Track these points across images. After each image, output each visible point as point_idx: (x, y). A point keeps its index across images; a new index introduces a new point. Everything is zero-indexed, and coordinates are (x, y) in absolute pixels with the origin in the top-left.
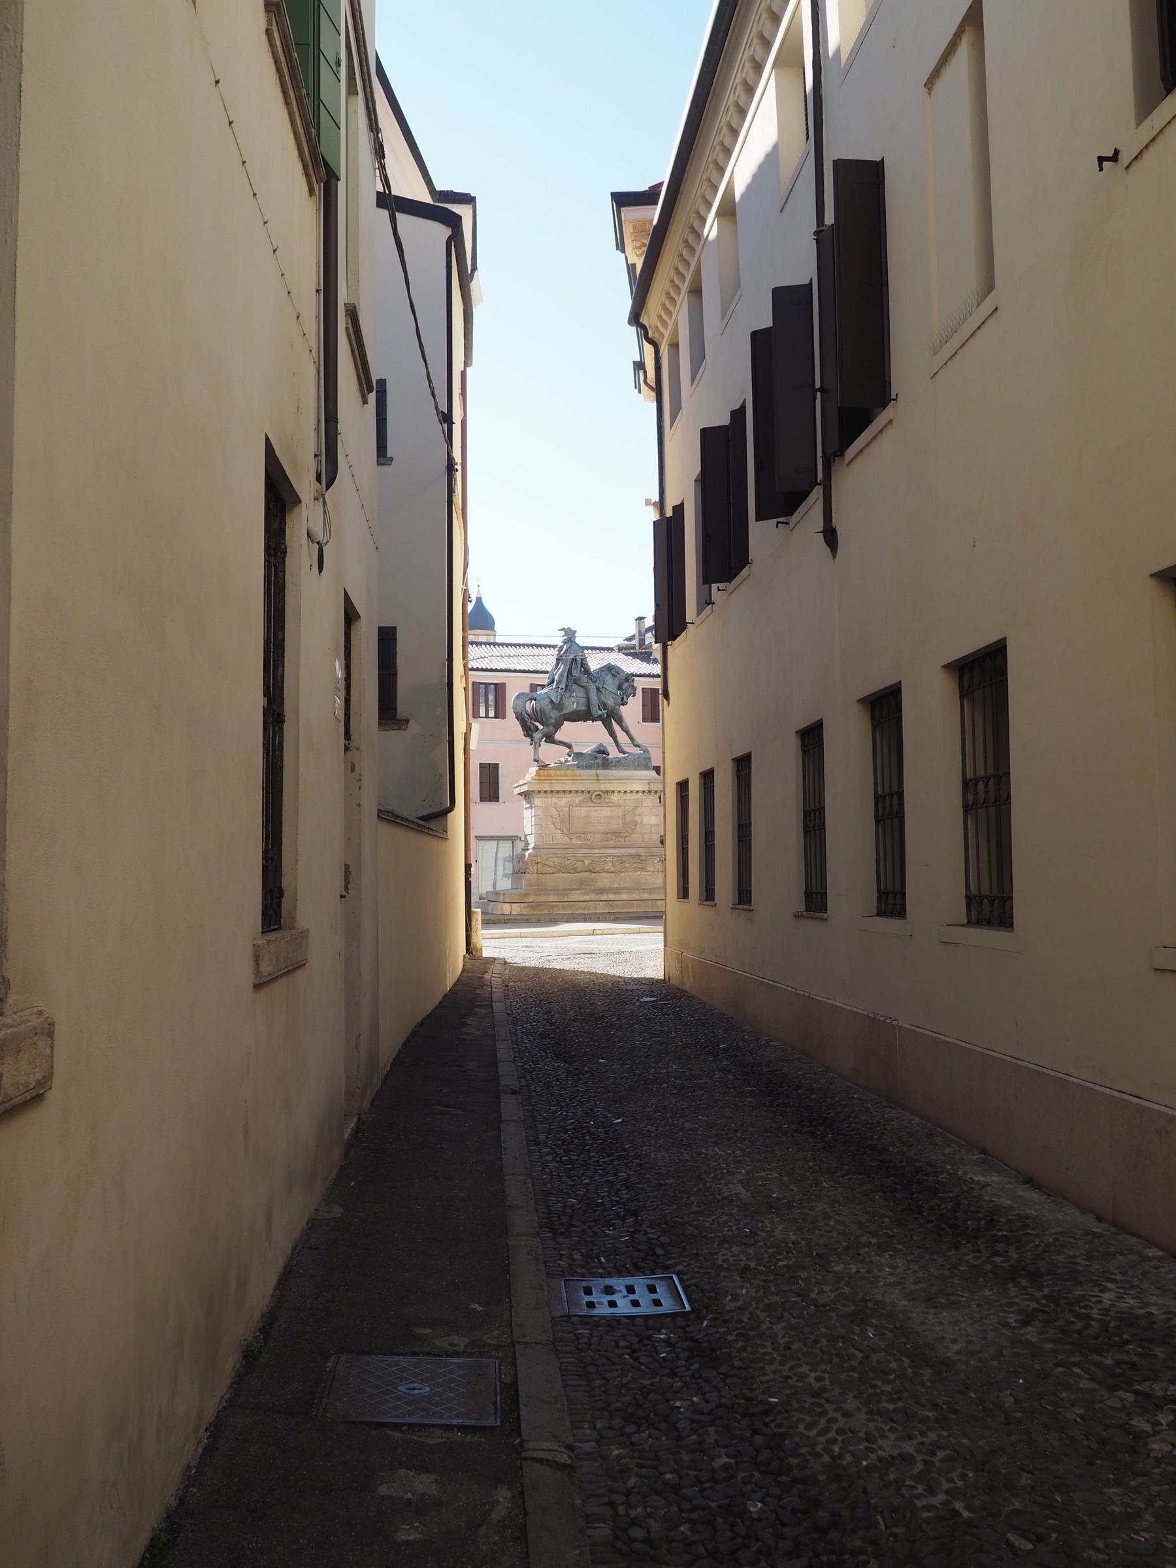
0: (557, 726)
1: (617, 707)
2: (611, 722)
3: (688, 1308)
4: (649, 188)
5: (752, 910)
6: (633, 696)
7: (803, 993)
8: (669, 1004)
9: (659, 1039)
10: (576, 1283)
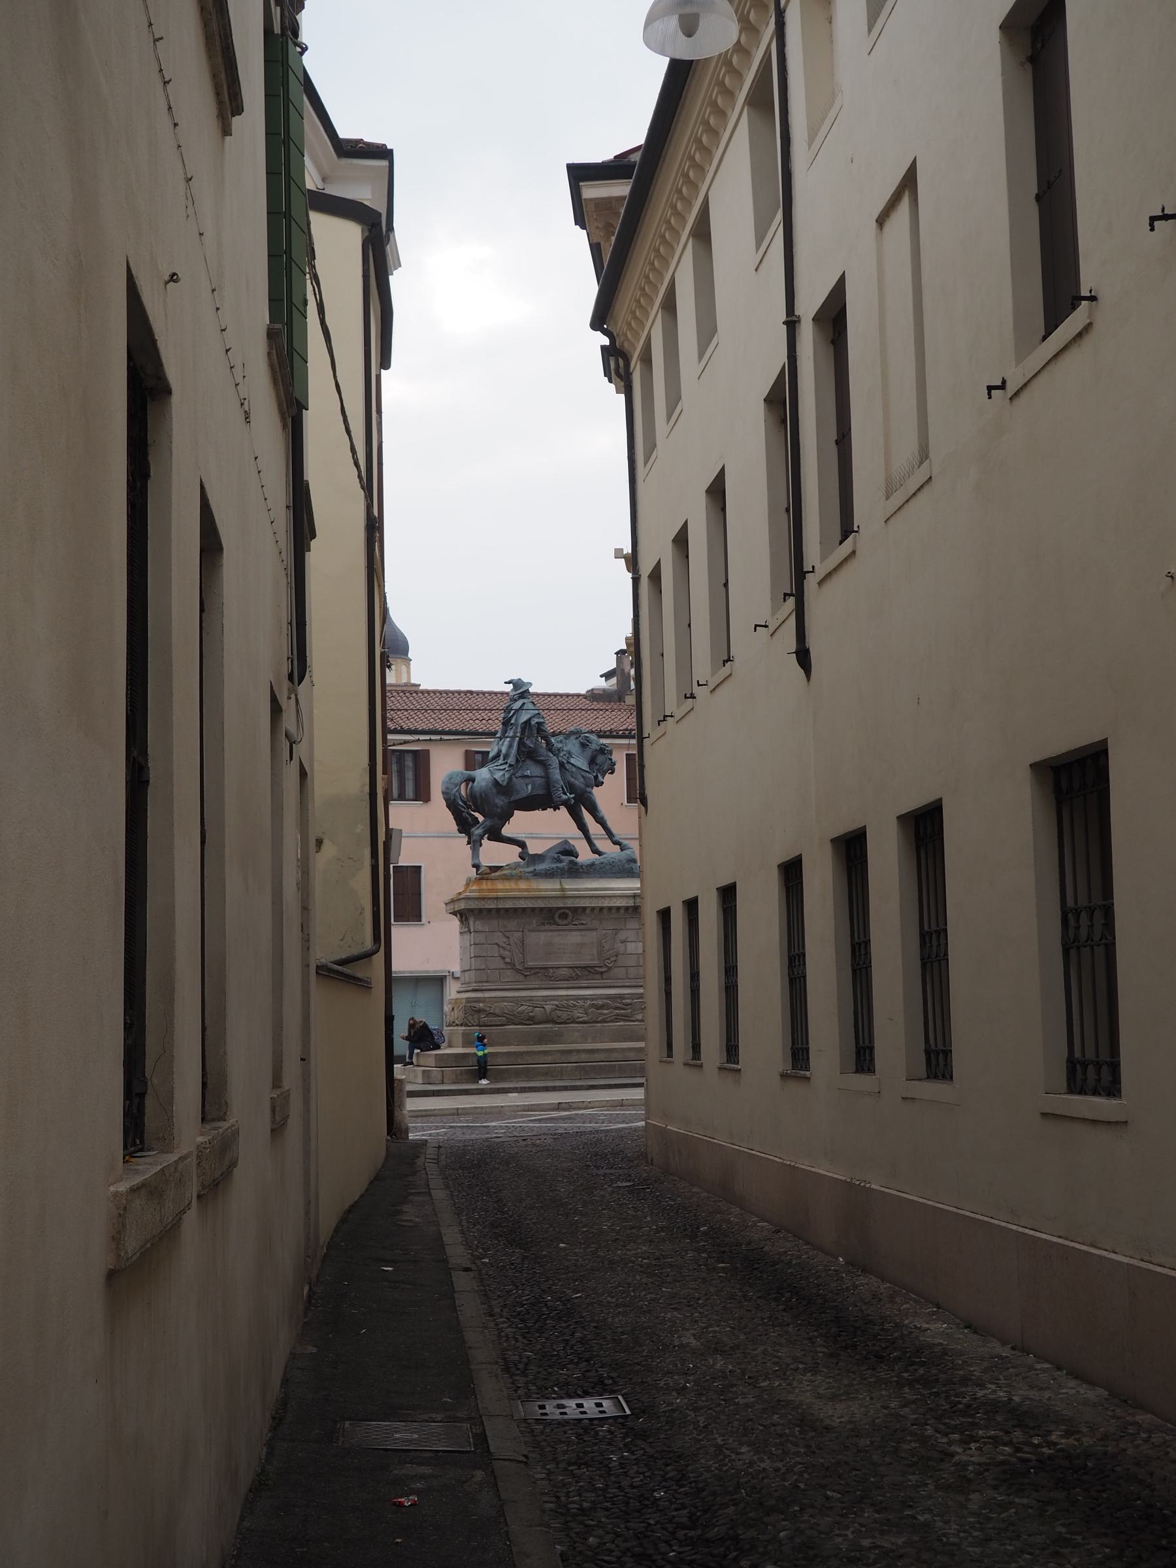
0: (506, 817)
1: (588, 789)
2: (581, 810)
3: (628, 1412)
4: (615, 157)
5: (740, 1070)
6: (612, 773)
7: (788, 1163)
8: (648, 1188)
9: (631, 1224)
10: (533, 1403)
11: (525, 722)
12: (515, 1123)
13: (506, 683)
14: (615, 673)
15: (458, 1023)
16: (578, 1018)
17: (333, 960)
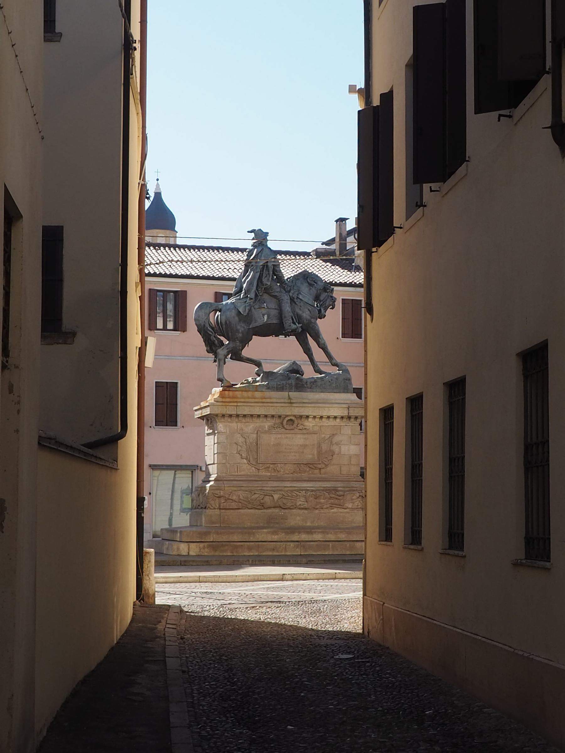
0: (246, 341)
1: (313, 320)
8: (368, 662)
11: (263, 266)
12: (246, 590)
13: (248, 232)
14: (334, 241)
15: (203, 506)
16: (300, 505)
17: (83, 443)
